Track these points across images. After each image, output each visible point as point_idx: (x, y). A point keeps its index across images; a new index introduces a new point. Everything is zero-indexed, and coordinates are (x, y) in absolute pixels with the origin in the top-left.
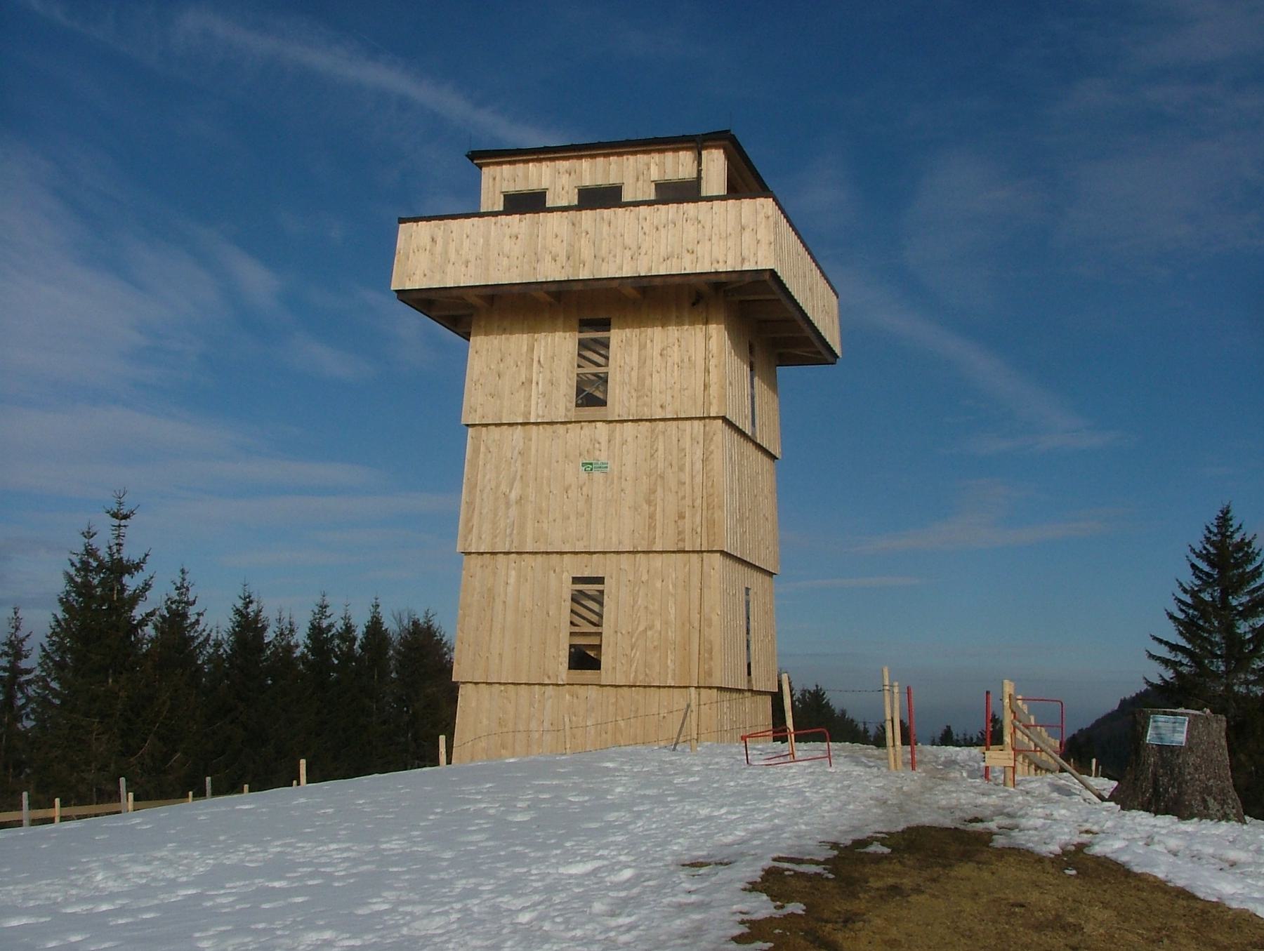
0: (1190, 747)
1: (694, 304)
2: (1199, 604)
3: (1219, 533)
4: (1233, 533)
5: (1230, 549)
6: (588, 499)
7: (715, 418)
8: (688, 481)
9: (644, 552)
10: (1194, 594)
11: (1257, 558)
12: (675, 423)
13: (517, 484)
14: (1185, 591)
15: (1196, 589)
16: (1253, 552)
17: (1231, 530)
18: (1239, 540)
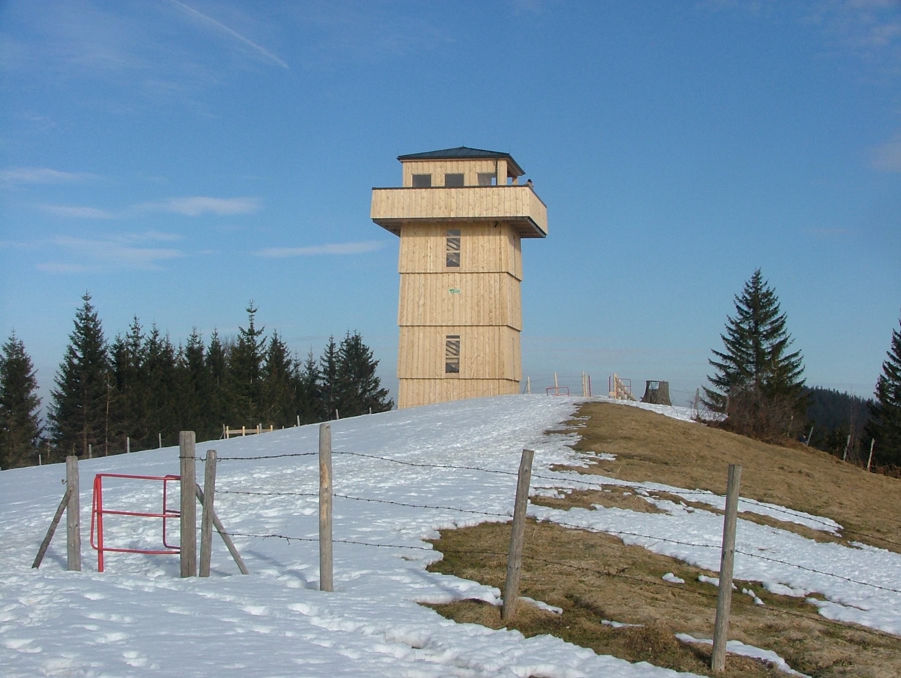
0: (659, 389)
1: (495, 226)
2: (740, 330)
3: (753, 287)
4: (761, 287)
5: (760, 296)
6: (453, 304)
7: (505, 272)
8: (493, 297)
10: (737, 324)
11: (776, 302)
12: (487, 274)
13: (422, 298)
14: (732, 323)
15: (738, 321)
16: (773, 298)
17: (760, 285)
18: (765, 291)
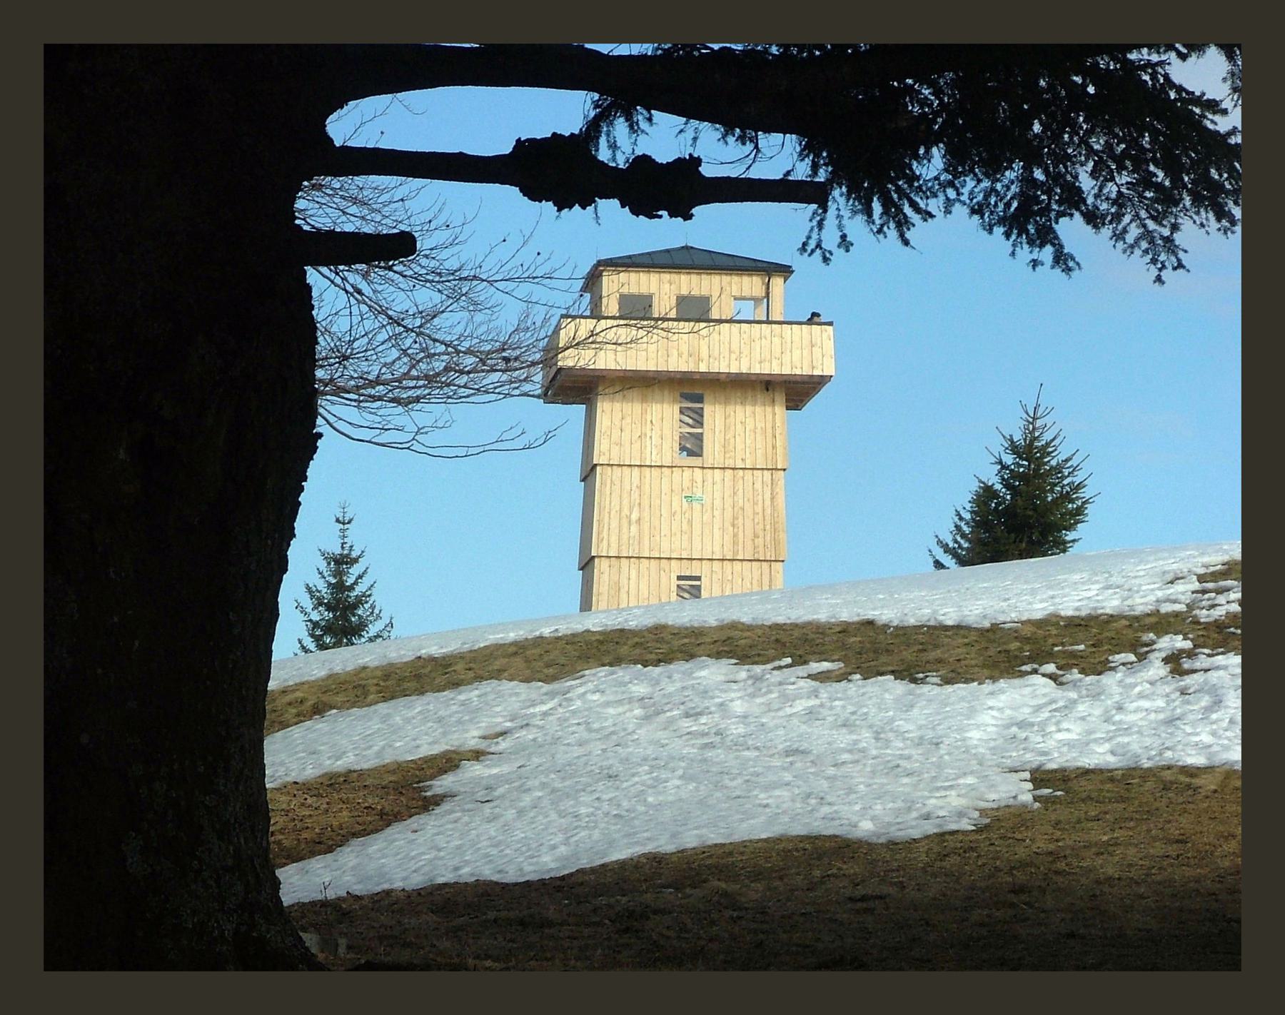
9: (729, 560)
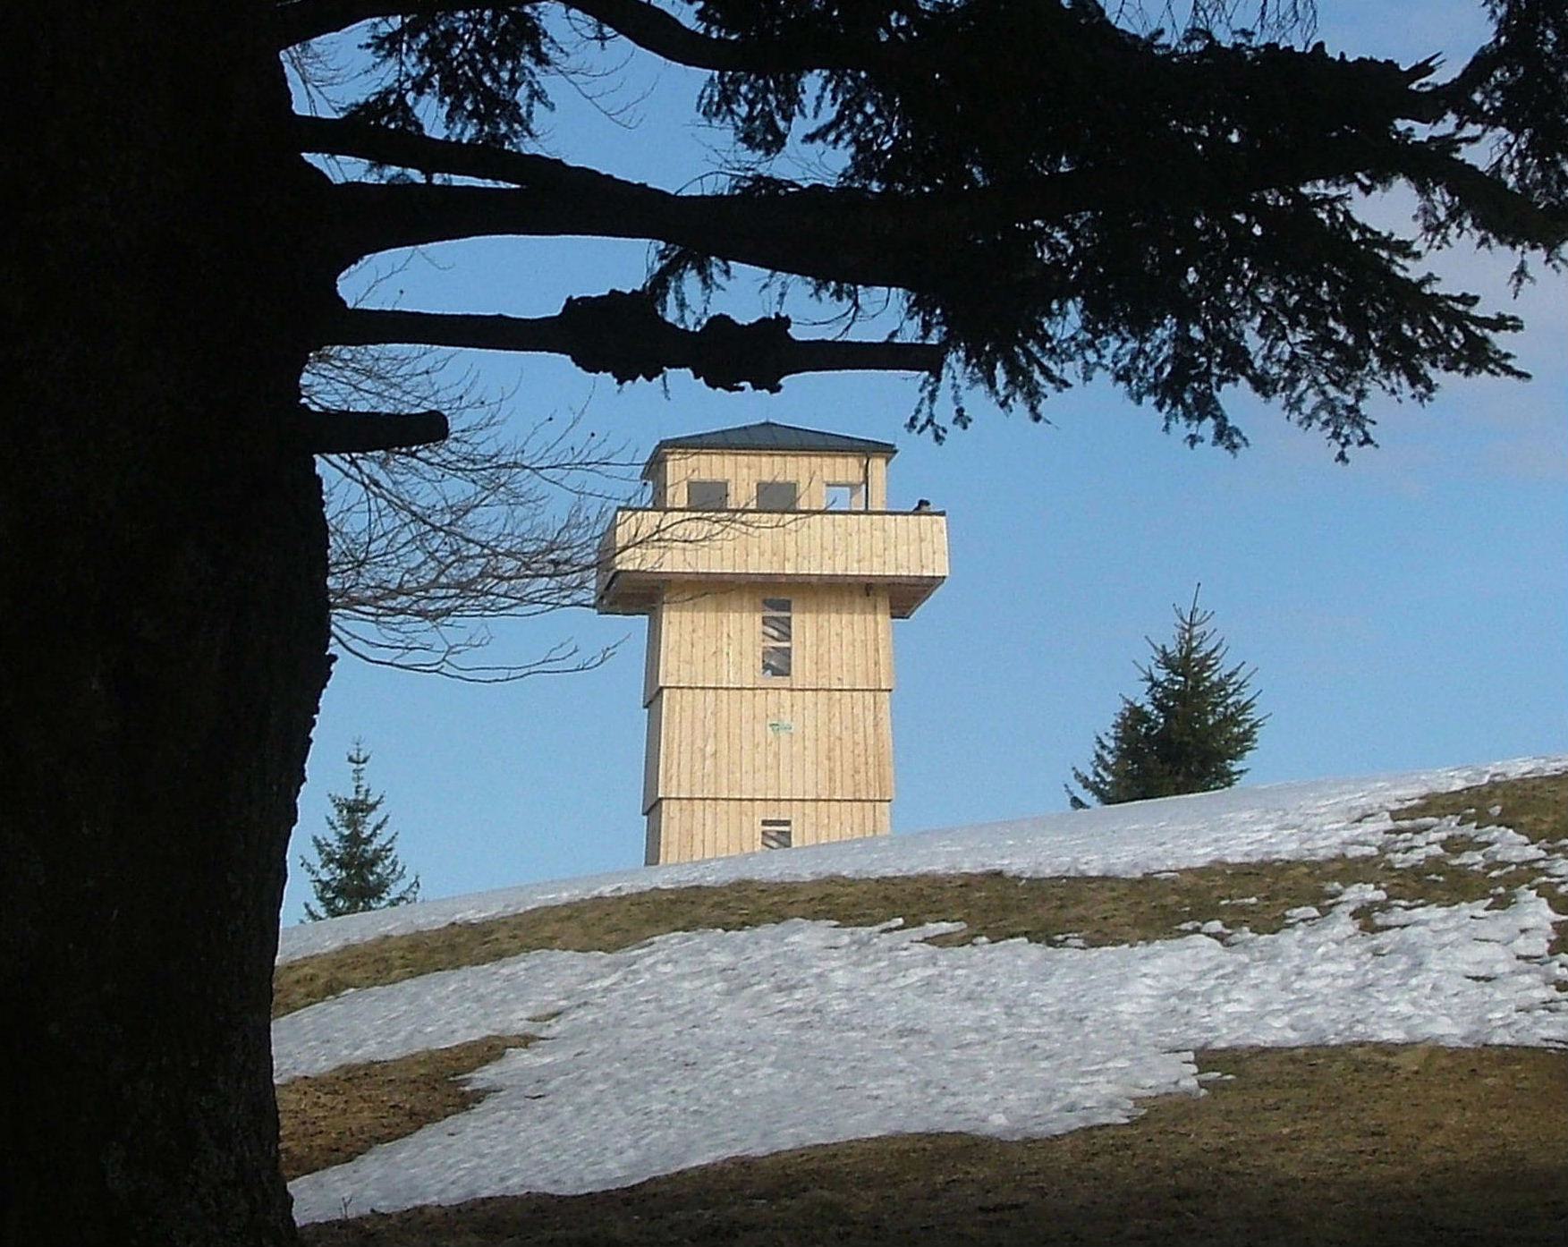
13: (711, 740)
